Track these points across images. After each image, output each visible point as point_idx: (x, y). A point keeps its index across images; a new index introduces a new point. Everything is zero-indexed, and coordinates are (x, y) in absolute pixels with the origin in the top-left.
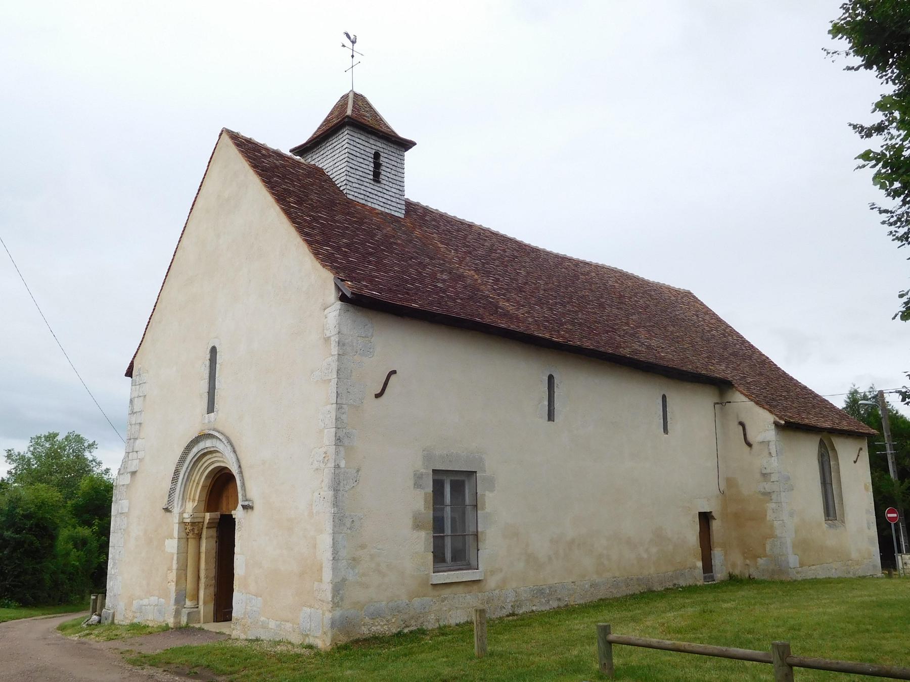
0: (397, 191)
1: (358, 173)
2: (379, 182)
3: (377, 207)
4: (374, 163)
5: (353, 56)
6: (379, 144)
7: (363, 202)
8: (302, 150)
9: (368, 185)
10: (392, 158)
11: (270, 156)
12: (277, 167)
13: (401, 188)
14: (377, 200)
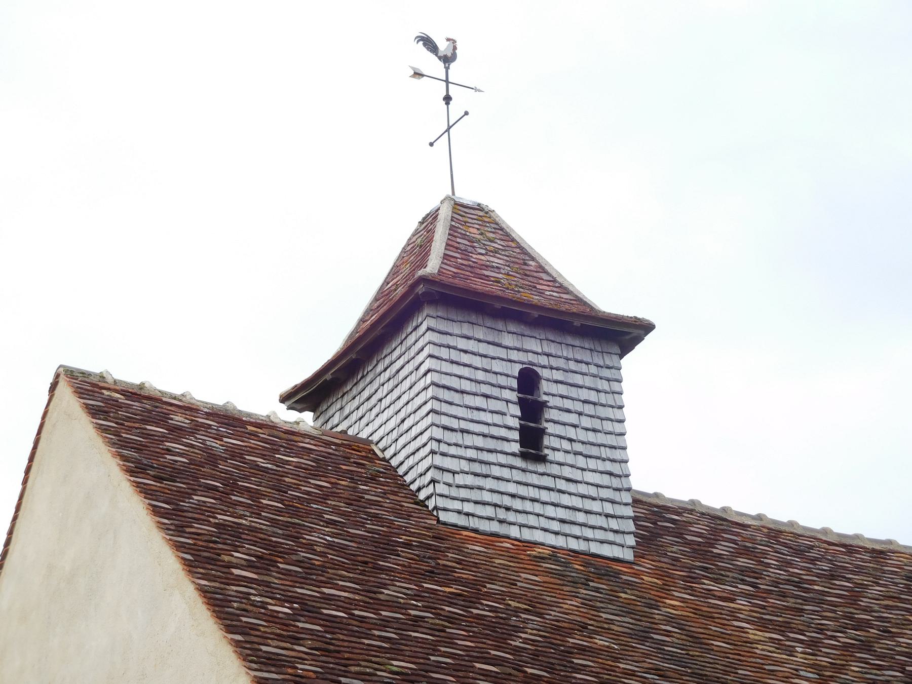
0: (605, 480)
1: (469, 440)
2: (542, 459)
3: (538, 536)
4: (521, 403)
5: (448, 99)
6: (533, 345)
7: (494, 527)
8: (314, 393)
9: (506, 473)
10: (578, 379)
11: (196, 428)
12: (212, 459)
13: (615, 468)
14: (552, 515)
